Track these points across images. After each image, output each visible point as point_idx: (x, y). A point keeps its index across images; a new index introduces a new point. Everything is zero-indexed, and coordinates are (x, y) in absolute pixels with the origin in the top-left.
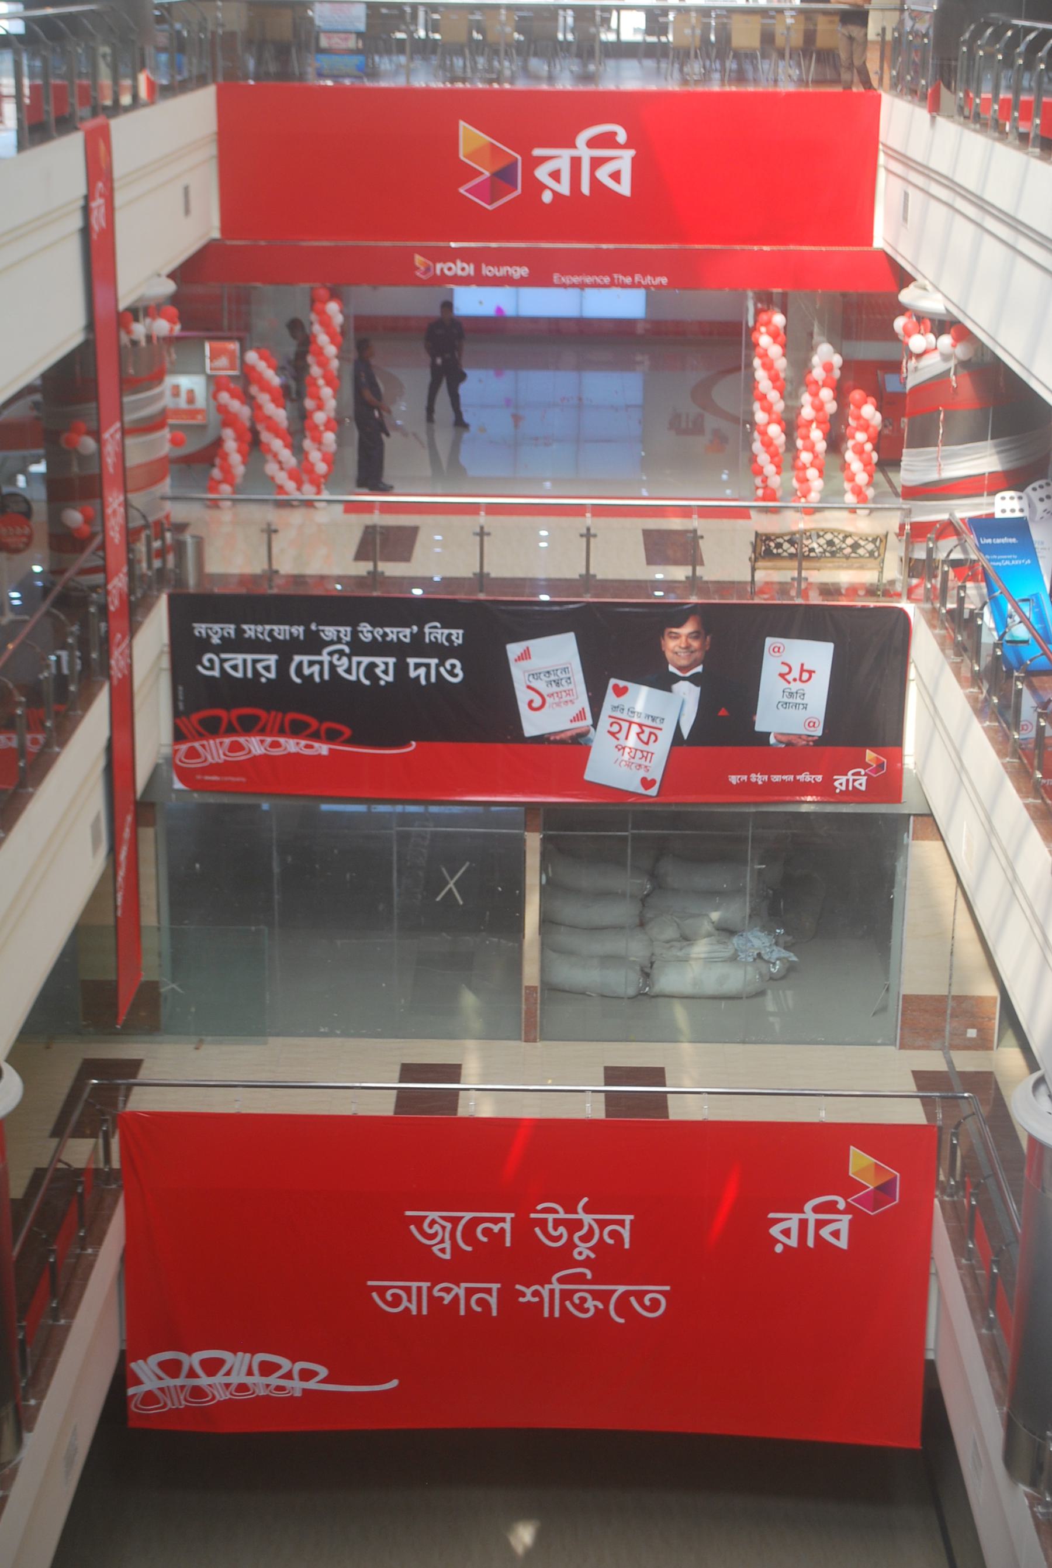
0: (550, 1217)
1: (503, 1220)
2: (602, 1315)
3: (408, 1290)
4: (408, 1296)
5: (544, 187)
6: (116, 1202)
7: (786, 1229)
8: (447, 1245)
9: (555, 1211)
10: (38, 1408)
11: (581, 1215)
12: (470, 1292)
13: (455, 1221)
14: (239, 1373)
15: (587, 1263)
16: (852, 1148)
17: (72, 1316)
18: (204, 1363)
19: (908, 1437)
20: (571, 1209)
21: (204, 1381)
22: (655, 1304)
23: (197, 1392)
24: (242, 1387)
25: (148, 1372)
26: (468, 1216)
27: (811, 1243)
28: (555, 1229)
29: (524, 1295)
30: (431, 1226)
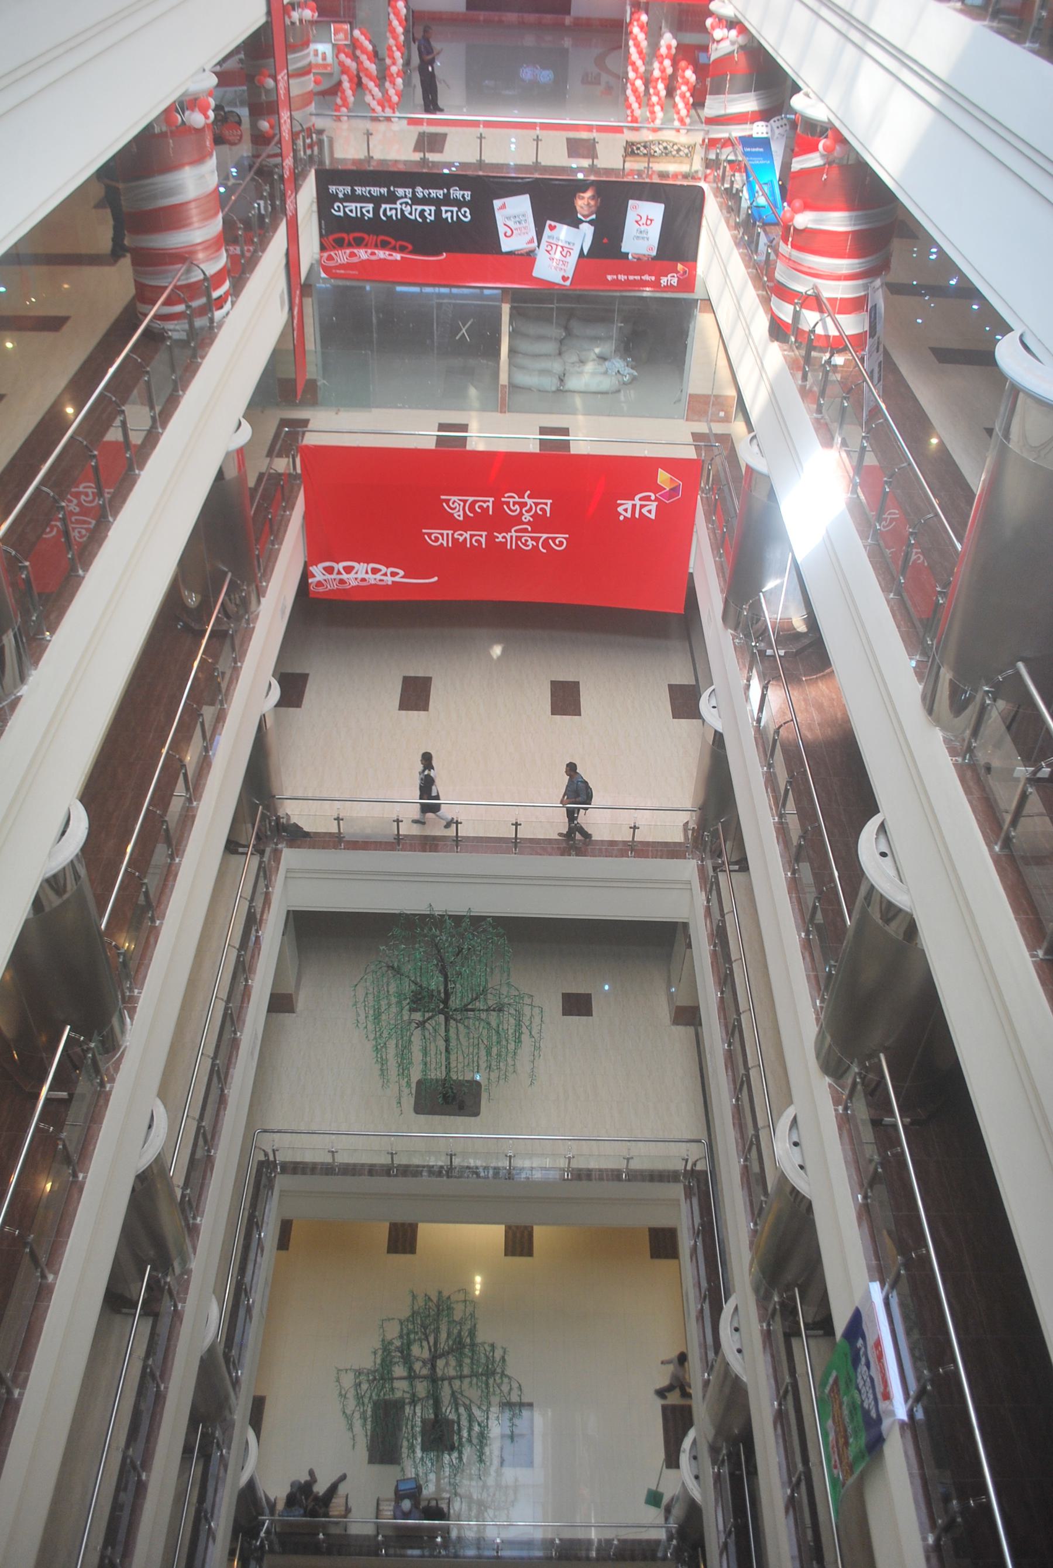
0: (511, 500)
2: (535, 548)
3: (442, 535)
4: (441, 537)
7: (625, 508)
8: (461, 513)
10: (267, 586)
11: (526, 500)
12: (472, 536)
13: (465, 502)
14: (361, 573)
17: (281, 544)
18: (344, 568)
21: (345, 576)
22: (561, 543)
23: (342, 581)
24: (363, 580)
25: (318, 572)
26: (471, 499)
27: (637, 516)
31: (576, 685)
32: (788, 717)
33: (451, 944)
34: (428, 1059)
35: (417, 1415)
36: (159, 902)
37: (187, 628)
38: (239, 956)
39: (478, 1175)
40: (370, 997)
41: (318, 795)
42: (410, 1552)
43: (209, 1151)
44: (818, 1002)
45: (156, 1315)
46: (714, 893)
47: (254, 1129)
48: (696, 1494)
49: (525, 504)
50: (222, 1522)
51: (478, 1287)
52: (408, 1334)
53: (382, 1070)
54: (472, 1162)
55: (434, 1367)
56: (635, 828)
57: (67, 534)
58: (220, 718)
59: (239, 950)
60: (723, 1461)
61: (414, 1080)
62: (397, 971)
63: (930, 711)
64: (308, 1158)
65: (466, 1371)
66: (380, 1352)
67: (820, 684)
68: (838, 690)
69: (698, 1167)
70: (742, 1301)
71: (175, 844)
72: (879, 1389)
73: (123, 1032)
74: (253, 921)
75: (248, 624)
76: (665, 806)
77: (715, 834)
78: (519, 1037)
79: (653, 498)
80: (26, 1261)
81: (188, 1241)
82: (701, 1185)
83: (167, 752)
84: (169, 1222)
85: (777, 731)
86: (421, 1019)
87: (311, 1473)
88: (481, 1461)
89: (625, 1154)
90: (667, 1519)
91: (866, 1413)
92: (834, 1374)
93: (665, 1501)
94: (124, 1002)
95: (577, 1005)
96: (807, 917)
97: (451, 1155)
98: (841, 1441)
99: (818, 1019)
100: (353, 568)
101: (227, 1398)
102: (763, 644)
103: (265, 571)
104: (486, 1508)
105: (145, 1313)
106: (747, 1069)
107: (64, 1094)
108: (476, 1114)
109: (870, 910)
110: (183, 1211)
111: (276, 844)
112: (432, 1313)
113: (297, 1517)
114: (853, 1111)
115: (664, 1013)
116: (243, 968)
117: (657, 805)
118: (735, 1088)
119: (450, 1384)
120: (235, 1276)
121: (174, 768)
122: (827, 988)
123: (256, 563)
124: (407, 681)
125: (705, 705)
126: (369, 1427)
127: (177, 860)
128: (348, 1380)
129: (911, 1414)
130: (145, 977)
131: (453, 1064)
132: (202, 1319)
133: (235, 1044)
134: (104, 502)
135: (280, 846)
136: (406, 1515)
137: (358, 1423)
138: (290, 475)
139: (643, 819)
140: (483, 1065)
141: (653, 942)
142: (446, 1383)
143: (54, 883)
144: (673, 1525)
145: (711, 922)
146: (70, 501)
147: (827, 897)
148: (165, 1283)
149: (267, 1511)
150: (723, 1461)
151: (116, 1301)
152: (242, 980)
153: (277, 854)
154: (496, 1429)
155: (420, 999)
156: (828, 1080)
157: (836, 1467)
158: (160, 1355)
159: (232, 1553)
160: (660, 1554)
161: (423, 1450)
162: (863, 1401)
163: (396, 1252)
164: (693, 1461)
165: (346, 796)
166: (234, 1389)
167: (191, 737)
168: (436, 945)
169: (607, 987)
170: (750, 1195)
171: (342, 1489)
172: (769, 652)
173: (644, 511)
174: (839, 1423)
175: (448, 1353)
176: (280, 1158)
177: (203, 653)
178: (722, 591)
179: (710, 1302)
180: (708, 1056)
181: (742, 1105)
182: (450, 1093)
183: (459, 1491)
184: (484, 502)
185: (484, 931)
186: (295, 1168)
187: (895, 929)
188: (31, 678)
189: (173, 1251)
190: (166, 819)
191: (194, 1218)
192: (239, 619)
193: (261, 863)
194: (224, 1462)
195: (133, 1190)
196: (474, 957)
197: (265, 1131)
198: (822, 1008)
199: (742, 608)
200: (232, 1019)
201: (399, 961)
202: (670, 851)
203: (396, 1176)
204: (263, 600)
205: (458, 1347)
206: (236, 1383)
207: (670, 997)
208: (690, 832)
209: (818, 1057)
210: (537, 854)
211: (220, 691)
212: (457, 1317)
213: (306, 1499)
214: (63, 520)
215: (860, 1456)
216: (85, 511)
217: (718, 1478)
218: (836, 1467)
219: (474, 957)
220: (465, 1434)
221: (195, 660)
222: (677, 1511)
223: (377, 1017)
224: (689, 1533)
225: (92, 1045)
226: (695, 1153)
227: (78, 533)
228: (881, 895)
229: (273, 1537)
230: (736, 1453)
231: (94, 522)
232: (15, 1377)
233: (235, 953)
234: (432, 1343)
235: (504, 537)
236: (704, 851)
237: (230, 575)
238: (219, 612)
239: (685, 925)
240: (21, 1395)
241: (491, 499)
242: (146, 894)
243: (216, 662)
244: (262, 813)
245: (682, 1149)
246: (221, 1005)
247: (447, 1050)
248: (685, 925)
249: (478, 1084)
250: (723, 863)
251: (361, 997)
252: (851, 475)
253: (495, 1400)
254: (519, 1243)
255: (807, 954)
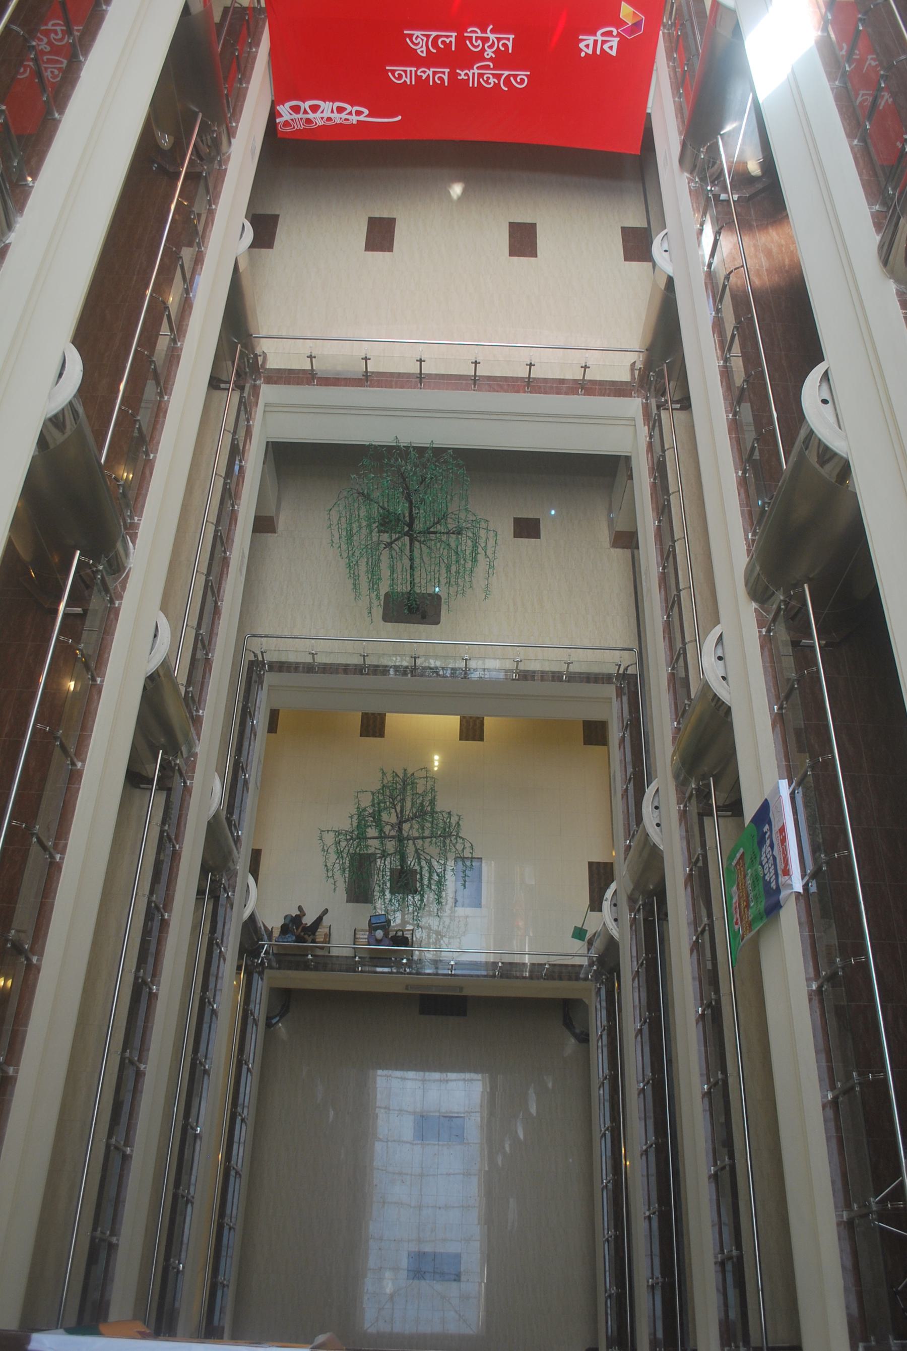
0: (474, 35)
1: (451, 36)
2: (497, 85)
3: (405, 72)
4: (403, 75)
5: (581, 50)
6: (264, 24)
7: (587, 44)
8: (424, 49)
9: (476, 32)
10: (237, 127)
11: (489, 34)
12: (435, 73)
13: (428, 37)
14: (327, 112)
15: (491, 59)
16: (623, 3)
17: (248, 82)
18: (311, 107)
19: (635, 149)
20: (484, 31)
21: (311, 116)
22: (522, 80)
23: (308, 121)
24: (329, 119)
25: (284, 110)
26: (434, 34)
27: (598, 52)
28: (476, 41)
29: (460, 75)
30: (416, 39)
31: (533, 226)
32: (738, 263)
33: (415, 473)
34: (395, 575)
35: (385, 866)
36: (152, 438)
37: (162, 170)
38: (225, 484)
39: (437, 673)
40: (343, 520)
41: (291, 334)
42: (379, 969)
43: (207, 654)
44: (750, 535)
45: (169, 790)
46: (657, 429)
47: (245, 633)
48: (615, 933)
49: (488, 39)
50: (231, 947)
51: (436, 763)
52: (379, 804)
53: (354, 584)
54: (433, 663)
55: (400, 830)
56: (585, 367)
57: (39, 74)
58: (198, 260)
59: (226, 478)
60: (639, 910)
61: (382, 593)
62: (367, 497)
63: (885, 262)
64: (292, 658)
65: (427, 833)
66: (356, 817)
67: (771, 231)
68: (792, 240)
69: (629, 672)
70: (663, 787)
71: (164, 384)
72: (780, 866)
73: (127, 554)
74: (236, 452)
75: (220, 166)
76: (613, 347)
77: (660, 375)
78: (476, 557)
79: (615, 33)
80: (57, 751)
81: (192, 729)
82: (631, 686)
83: (151, 295)
84: (175, 712)
85: (727, 277)
86: (389, 541)
87: (300, 908)
88: (439, 903)
89: (566, 659)
90: (589, 950)
91: (767, 884)
92: (741, 850)
93: (588, 936)
94: (126, 528)
95: (527, 528)
96: (745, 457)
97: (415, 658)
98: (743, 904)
99: (749, 551)
100: (318, 107)
101: (230, 853)
102: (717, 188)
103: (234, 110)
104: (442, 937)
105: (160, 788)
106: (679, 590)
107: (79, 610)
108: (437, 622)
109: (807, 453)
110: (187, 706)
111: (255, 380)
112: (399, 787)
113: (290, 942)
114: (775, 633)
115: (605, 537)
116: (230, 494)
117: (606, 346)
118: (667, 607)
119: (414, 843)
120: (233, 755)
121: (158, 309)
122: (759, 523)
123: (225, 101)
124: (372, 222)
125: (657, 249)
126: (347, 876)
127: (166, 398)
128: (329, 839)
129: (806, 887)
130: (143, 506)
131: (417, 580)
132: (207, 791)
133: (225, 562)
134: (74, 40)
135: (258, 382)
136: (379, 942)
137: (338, 874)
138: (254, 8)
139: (592, 358)
140: (443, 581)
141: (595, 474)
142: (411, 842)
143: (56, 422)
144: (594, 954)
145: (652, 456)
146: (41, 40)
147: (765, 438)
148: (176, 764)
149: (266, 937)
150: (639, 910)
151: (135, 778)
152: (229, 505)
153: (256, 390)
154: (451, 883)
155: (388, 523)
156: (754, 605)
157: (737, 923)
158: (175, 820)
159: (239, 968)
160: (582, 976)
161: (392, 893)
162: (765, 875)
163: (367, 736)
164: (614, 908)
165: (319, 336)
166: (236, 845)
167: (172, 280)
168: (402, 474)
169: (553, 512)
170: (675, 699)
171: (326, 921)
172: (723, 196)
173: (606, 47)
174: (742, 888)
175: (412, 819)
176: (268, 658)
177: (179, 196)
178: (680, 133)
179: (634, 785)
180: (643, 577)
181: (673, 621)
182: (414, 605)
183: (420, 924)
184: (447, 37)
185: (445, 462)
186: (281, 667)
187: (829, 472)
188: (18, 226)
189: (180, 737)
190: (154, 359)
191: (197, 711)
192: (211, 160)
193: (241, 398)
194: (230, 902)
195: (145, 688)
196: (436, 486)
197: (254, 636)
198: (753, 541)
199: (699, 151)
200: (221, 541)
201: (369, 489)
202: (617, 389)
203: (367, 674)
204: (233, 140)
205: (421, 814)
206: (237, 840)
207: (611, 522)
208: (637, 373)
209: (746, 585)
210: (495, 391)
211: (197, 233)
212: (420, 790)
213: (297, 929)
214: (35, 60)
215: (759, 917)
216: (56, 50)
217: (634, 921)
218: (737, 923)
219: (436, 486)
220: (426, 882)
221: (172, 202)
222: (598, 944)
223: (350, 537)
224: (607, 961)
225: (101, 568)
226: (627, 659)
227: (51, 73)
228: (820, 440)
229: (271, 956)
230: (650, 903)
231: (65, 62)
232: (55, 845)
233: (222, 480)
234: (398, 811)
235: (466, 74)
236: (649, 390)
237: (200, 115)
238: (192, 154)
239: (628, 459)
240: (62, 859)
241: (454, 34)
242: (140, 429)
243: (192, 204)
244: (241, 351)
245: (616, 656)
246: (211, 529)
247: (412, 567)
248: (628, 459)
249: (438, 597)
250: (666, 401)
251: (335, 520)
252: (823, 10)
253: (451, 856)
254: (472, 730)
255: (742, 491)
